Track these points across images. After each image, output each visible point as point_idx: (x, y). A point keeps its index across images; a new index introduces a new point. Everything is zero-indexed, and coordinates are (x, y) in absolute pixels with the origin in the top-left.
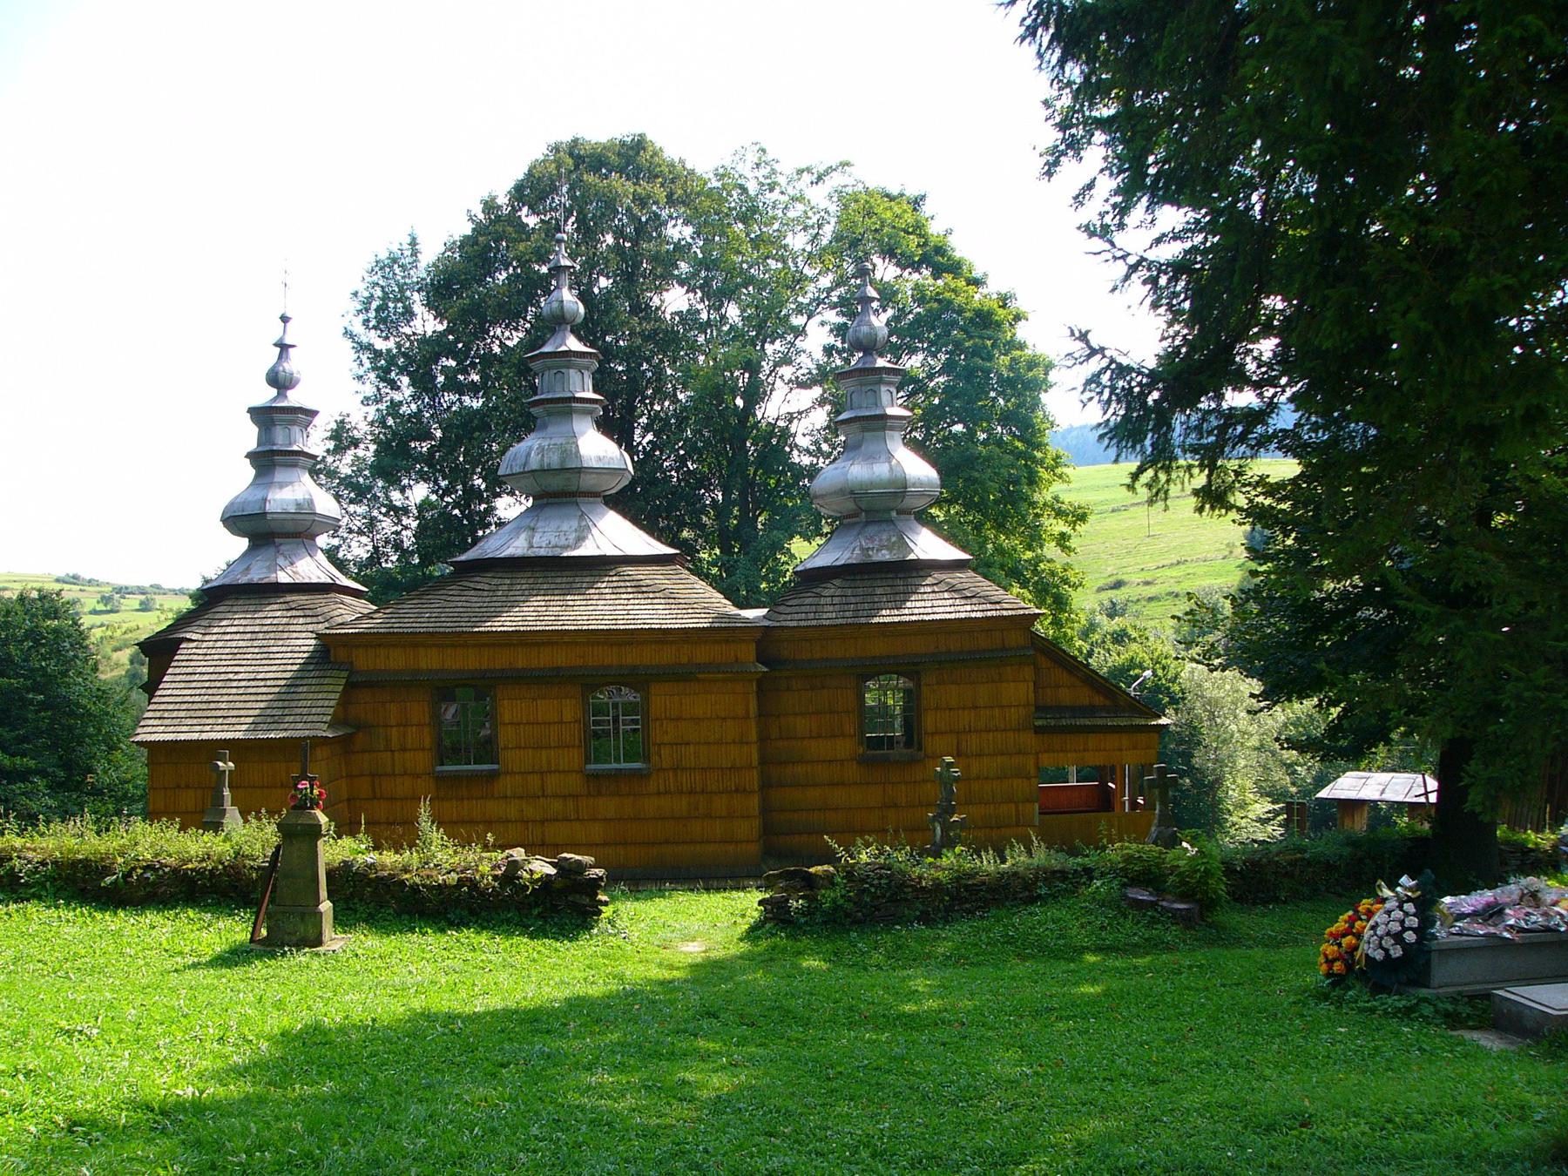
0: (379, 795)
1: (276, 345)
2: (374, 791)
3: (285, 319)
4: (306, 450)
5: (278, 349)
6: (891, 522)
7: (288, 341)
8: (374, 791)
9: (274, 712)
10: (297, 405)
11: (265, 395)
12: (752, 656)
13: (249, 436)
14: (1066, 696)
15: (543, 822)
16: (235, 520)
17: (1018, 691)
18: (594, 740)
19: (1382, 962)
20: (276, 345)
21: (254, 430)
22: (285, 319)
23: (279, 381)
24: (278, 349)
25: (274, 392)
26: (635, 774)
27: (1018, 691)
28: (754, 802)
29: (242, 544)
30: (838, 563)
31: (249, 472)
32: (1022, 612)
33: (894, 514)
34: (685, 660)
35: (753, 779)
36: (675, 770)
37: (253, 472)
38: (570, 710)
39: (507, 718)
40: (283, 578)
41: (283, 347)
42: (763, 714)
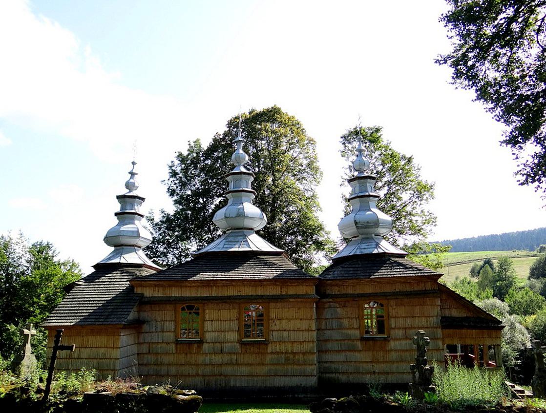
0: (151, 352)
1: (129, 173)
2: (149, 350)
3: (134, 163)
4: (138, 212)
5: (130, 175)
6: (372, 238)
7: (134, 172)
8: (149, 350)
9: (100, 311)
10: (136, 195)
11: (124, 191)
12: (314, 292)
13: (117, 208)
14: (455, 313)
15: (221, 365)
16: (108, 240)
17: (434, 310)
18: (245, 329)
19: (83, 402)
20: (129, 173)
21: (119, 205)
22: (134, 163)
23: (129, 186)
24: (130, 175)
25: (128, 191)
26: (260, 343)
27: (434, 310)
28: (315, 358)
29: (113, 249)
30: (351, 254)
31: (115, 221)
32: (433, 274)
33: (373, 235)
34: (284, 293)
35: (313, 346)
36: (280, 342)
37: (117, 221)
38: (234, 313)
39: (207, 317)
40: (123, 261)
41: (132, 174)
42: (319, 319)
